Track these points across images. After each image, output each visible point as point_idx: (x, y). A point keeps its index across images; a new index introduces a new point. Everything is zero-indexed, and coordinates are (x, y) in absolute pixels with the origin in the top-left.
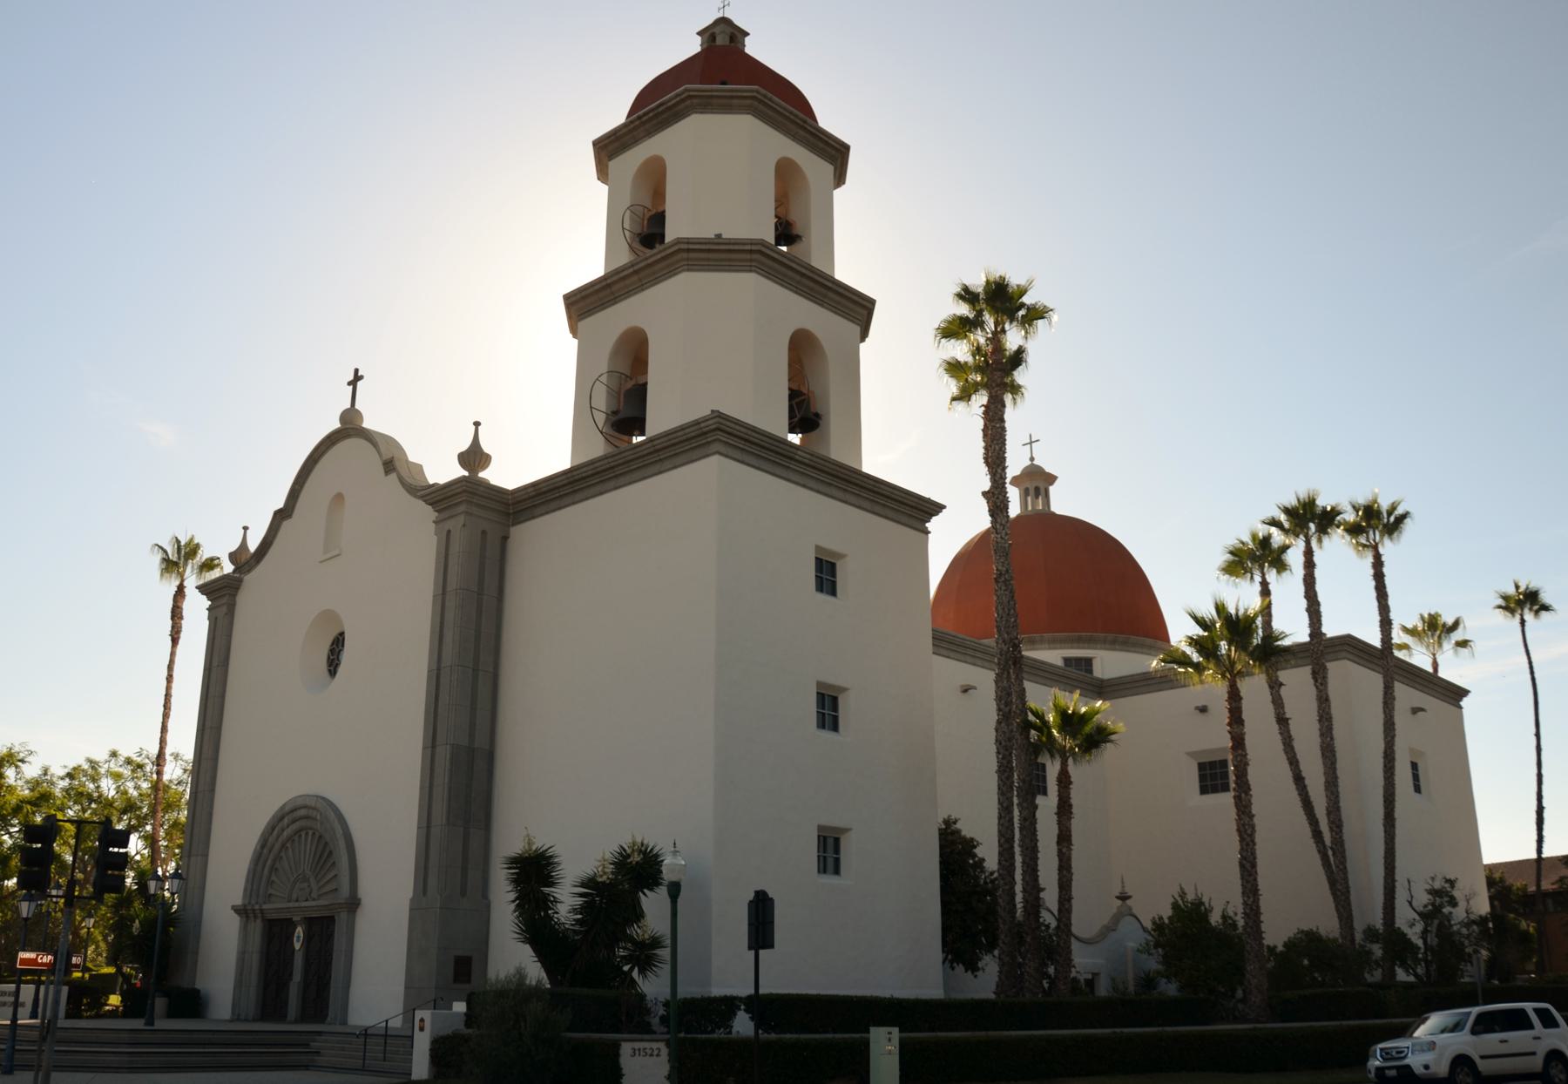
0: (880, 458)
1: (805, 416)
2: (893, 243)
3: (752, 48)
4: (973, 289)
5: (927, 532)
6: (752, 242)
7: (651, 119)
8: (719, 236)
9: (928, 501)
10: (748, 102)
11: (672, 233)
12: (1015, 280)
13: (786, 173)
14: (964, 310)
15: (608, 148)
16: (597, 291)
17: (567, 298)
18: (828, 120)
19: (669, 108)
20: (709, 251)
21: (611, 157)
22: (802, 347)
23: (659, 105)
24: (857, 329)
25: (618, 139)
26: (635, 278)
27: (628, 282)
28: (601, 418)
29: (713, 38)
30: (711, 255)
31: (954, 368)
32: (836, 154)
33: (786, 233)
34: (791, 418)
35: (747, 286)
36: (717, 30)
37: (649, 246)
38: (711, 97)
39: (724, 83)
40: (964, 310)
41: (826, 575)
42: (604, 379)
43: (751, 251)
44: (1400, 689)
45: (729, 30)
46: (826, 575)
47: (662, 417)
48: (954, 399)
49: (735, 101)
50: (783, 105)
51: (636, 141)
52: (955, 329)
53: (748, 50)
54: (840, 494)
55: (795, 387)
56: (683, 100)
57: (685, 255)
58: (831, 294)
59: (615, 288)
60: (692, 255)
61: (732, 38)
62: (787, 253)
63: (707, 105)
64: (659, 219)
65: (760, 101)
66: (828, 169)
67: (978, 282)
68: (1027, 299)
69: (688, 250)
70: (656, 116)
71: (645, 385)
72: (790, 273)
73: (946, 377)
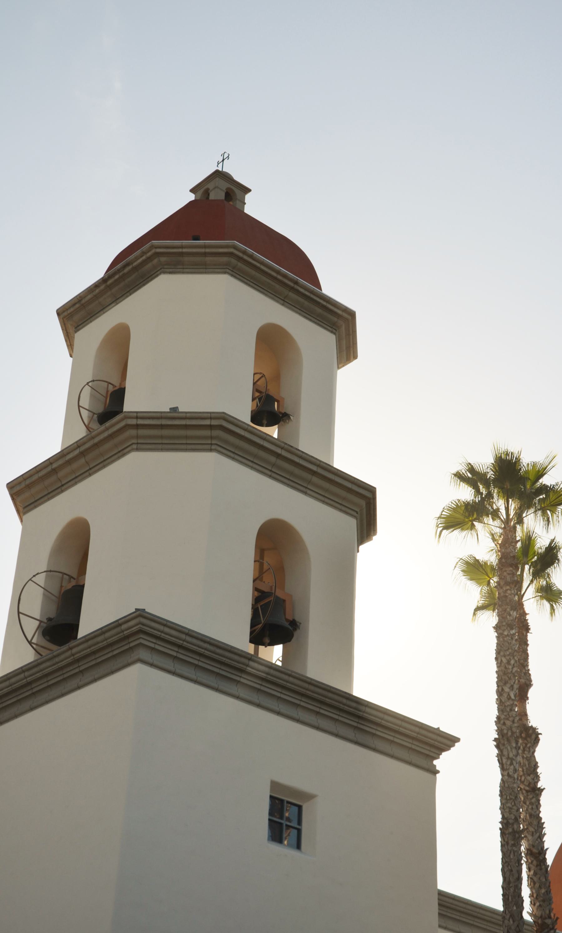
0: (373, 680)
1: (274, 619)
2: (397, 425)
3: (253, 207)
4: (477, 468)
5: (435, 772)
6: (212, 416)
7: (117, 282)
8: (174, 410)
9: (437, 732)
10: (225, 259)
11: (131, 404)
12: (528, 459)
13: (271, 342)
14: (466, 494)
15: (76, 315)
16: (42, 479)
17: (11, 486)
18: (332, 286)
19: (136, 269)
20: (162, 427)
21: (78, 328)
22: (275, 543)
23: (131, 270)
24: (349, 524)
25: (83, 306)
26: (82, 461)
27: (75, 465)
28: (31, 627)
29: (207, 193)
30: (165, 432)
31: (474, 569)
32: (338, 322)
33: (268, 409)
34: (253, 625)
35: (208, 467)
36: (210, 186)
37: (110, 425)
38: (182, 254)
39: (196, 238)
40: (466, 494)
41: (285, 818)
42: (41, 579)
43: (211, 427)
44: (265, 569)
45: (225, 185)
46: (285, 818)
47: (91, 621)
48: (478, 609)
49: (209, 259)
50: (280, 269)
51: (103, 309)
52: (461, 518)
53: (248, 210)
54: (311, 718)
55: (264, 588)
56: (150, 259)
57: (133, 432)
58: (315, 479)
59: (61, 474)
60: (141, 432)
61: (229, 195)
62: (269, 433)
63: (178, 264)
64: (118, 396)
65: (239, 259)
66: (327, 340)
67: (485, 461)
68: (546, 480)
69: (137, 426)
70: (123, 278)
71: (83, 586)
72: (262, 453)
73: (464, 580)
